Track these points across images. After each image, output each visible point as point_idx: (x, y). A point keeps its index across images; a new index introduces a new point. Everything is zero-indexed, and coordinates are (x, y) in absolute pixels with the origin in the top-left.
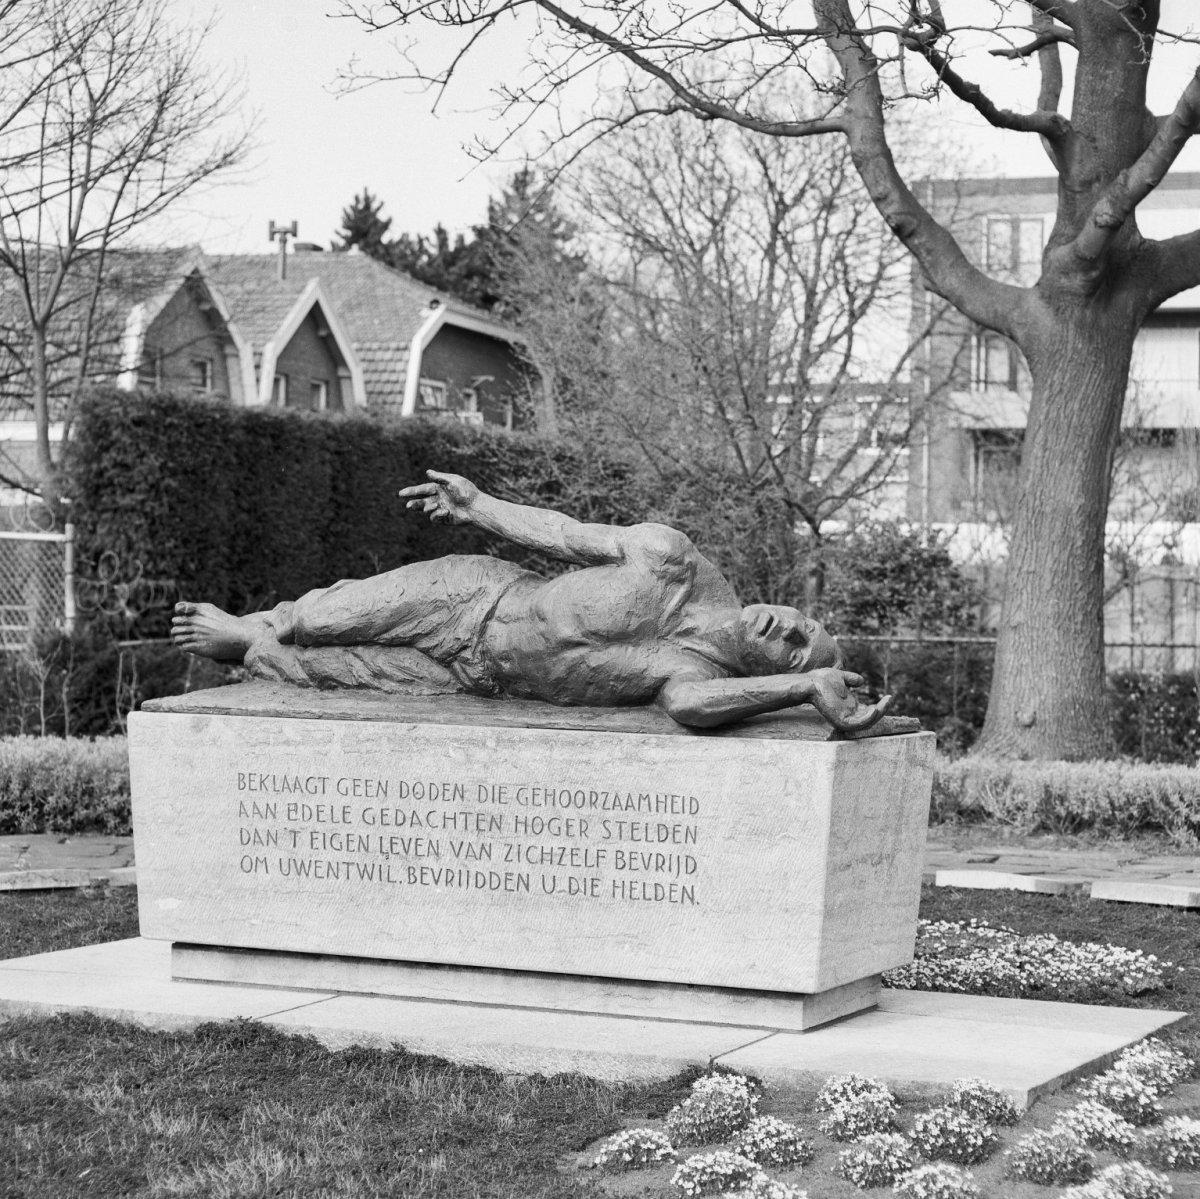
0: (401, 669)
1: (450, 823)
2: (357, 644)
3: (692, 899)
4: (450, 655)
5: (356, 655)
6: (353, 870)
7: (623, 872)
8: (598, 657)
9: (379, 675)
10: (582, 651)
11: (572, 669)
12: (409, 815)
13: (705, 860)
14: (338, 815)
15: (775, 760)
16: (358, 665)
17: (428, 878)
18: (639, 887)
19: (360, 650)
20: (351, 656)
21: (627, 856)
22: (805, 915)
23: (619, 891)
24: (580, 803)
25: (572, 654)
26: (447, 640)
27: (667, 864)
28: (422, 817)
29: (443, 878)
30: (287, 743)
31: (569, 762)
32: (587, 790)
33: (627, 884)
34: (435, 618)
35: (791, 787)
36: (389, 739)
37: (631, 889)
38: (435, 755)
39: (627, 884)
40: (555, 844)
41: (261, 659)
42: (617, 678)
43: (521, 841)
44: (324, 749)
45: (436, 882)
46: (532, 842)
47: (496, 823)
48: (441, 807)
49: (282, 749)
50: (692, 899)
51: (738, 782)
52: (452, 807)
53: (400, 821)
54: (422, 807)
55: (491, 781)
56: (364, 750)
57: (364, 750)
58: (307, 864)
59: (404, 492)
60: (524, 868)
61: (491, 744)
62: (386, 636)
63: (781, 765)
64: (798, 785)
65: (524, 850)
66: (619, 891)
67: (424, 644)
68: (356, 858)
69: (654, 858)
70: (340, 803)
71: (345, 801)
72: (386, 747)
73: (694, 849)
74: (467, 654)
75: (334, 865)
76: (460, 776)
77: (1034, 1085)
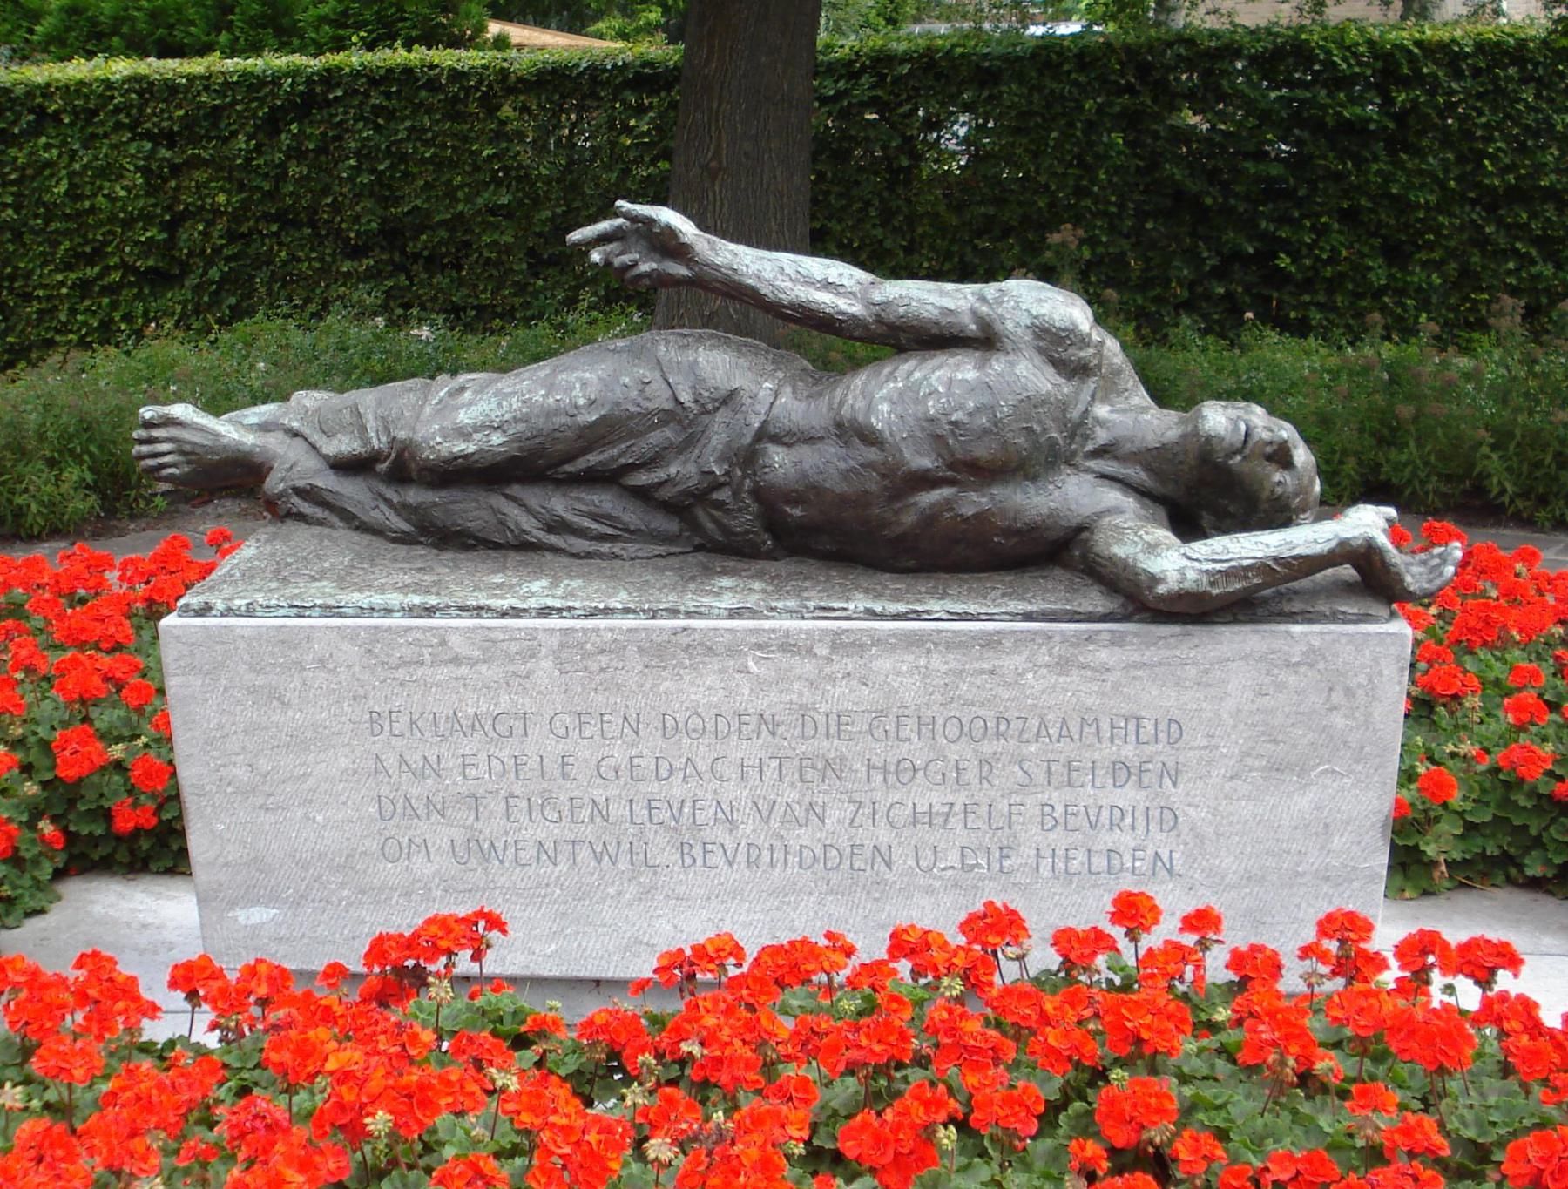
0: (596, 517)
1: (754, 773)
2: (510, 481)
3: (1170, 871)
4: (692, 495)
5: (507, 496)
6: (584, 853)
7: (1052, 836)
8: (974, 502)
9: (558, 526)
10: (946, 492)
11: (930, 518)
12: (679, 764)
13: (1191, 811)
14: (553, 769)
15: (1312, 657)
16: (513, 512)
17: (717, 859)
18: (1081, 856)
19: (515, 490)
20: (502, 499)
21: (1060, 810)
22: (1356, 885)
23: (1046, 864)
24: (977, 734)
25: (929, 498)
26: (681, 470)
27: (1128, 820)
28: (702, 767)
29: (742, 857)
30: (456, 660)
31: (959, 674)
32: (990, 714)
33: (1060, 852)
34: (656, 438)
35: (1337, 697)
36: (640, 650)
37: (1068, 859)
38: (722, 671)
39: (1060, 852)
40: (936, 799)
41: (298, 491)
42: (1009, 532)
43: (878, 795)
44: (522, 669)
45: (730, 864)
46: (896, 797)
47: (832, 768)
48: (738, 750)
49: (443, 673)
50: (1170, 871)
51: (1249, 694)
52: (750, 751)
53: (664, 773)
54: (703, 755)
55: (824, 708)
56: (595, 667)
57: (595, 667)
58: (499, 845)
59: (576, 236)
60: (884, 835)
61: (822, 650)
62: (569, 468)
63: (1321, 666)
64: (1349, 692)
65: (882, 808)
66: (1046, 864)
67: (642, 479)
68: (588, 832)
69: (1105, 813)
70: (554, 748)
71: (562, 747)
72: (635, 661)
73: (1176, 795)
74: (723, 495)
75: (549, 846)
76: (770, 702)
77: (1380, 860)
